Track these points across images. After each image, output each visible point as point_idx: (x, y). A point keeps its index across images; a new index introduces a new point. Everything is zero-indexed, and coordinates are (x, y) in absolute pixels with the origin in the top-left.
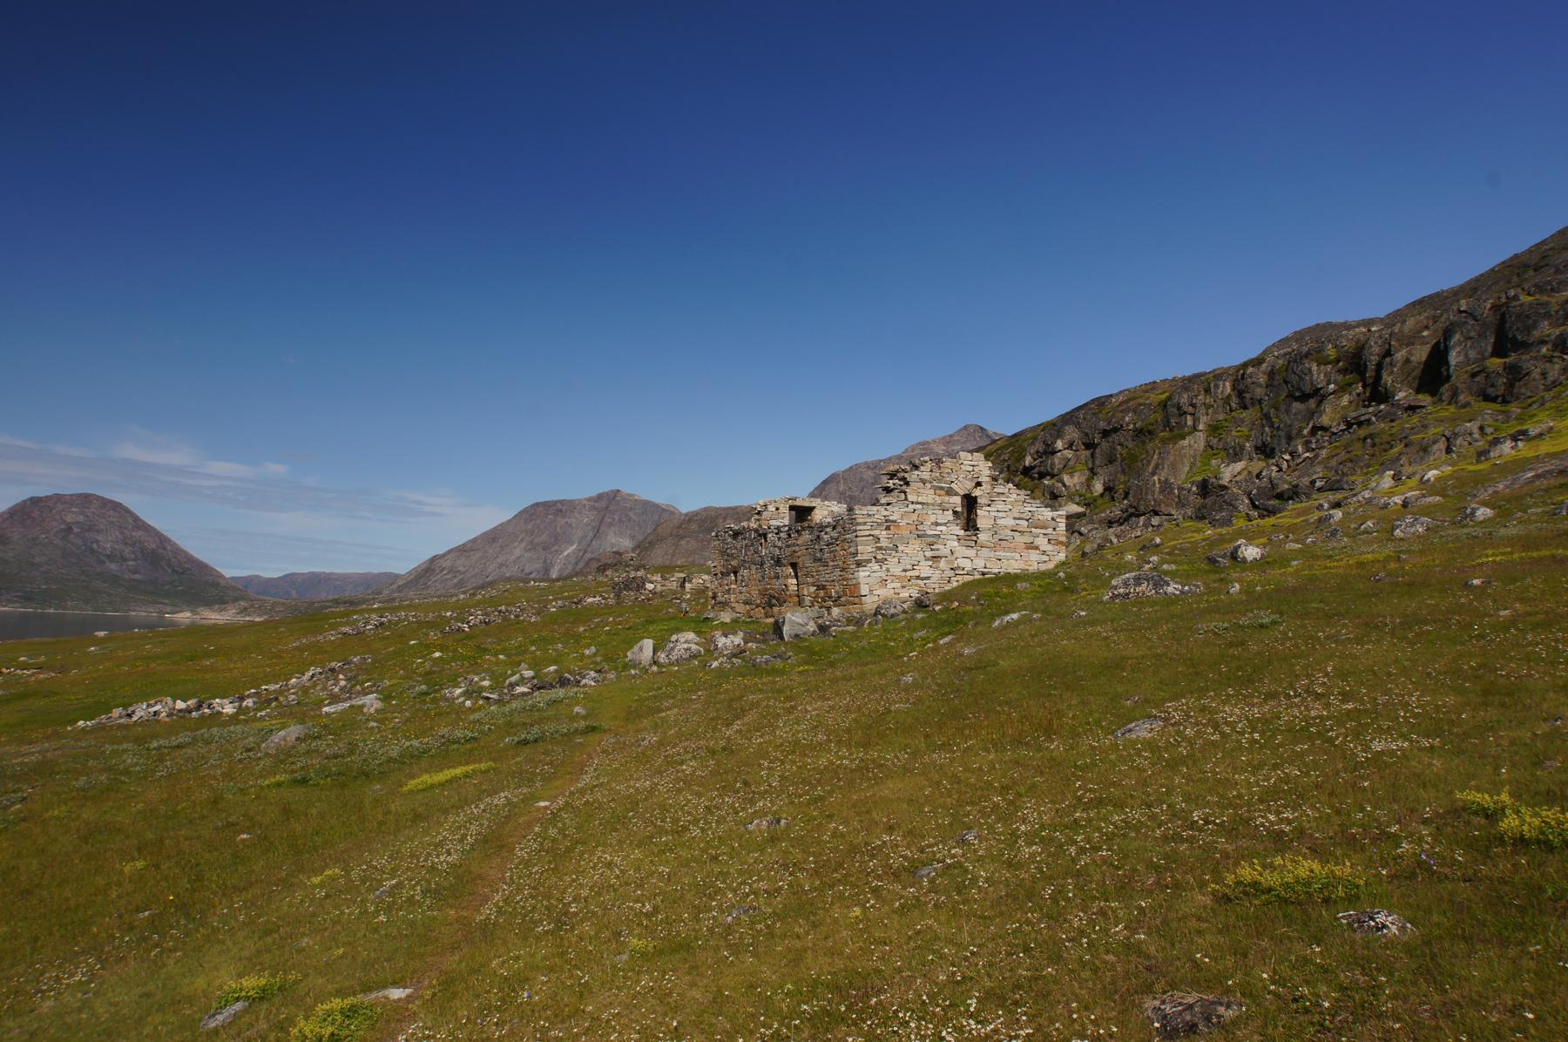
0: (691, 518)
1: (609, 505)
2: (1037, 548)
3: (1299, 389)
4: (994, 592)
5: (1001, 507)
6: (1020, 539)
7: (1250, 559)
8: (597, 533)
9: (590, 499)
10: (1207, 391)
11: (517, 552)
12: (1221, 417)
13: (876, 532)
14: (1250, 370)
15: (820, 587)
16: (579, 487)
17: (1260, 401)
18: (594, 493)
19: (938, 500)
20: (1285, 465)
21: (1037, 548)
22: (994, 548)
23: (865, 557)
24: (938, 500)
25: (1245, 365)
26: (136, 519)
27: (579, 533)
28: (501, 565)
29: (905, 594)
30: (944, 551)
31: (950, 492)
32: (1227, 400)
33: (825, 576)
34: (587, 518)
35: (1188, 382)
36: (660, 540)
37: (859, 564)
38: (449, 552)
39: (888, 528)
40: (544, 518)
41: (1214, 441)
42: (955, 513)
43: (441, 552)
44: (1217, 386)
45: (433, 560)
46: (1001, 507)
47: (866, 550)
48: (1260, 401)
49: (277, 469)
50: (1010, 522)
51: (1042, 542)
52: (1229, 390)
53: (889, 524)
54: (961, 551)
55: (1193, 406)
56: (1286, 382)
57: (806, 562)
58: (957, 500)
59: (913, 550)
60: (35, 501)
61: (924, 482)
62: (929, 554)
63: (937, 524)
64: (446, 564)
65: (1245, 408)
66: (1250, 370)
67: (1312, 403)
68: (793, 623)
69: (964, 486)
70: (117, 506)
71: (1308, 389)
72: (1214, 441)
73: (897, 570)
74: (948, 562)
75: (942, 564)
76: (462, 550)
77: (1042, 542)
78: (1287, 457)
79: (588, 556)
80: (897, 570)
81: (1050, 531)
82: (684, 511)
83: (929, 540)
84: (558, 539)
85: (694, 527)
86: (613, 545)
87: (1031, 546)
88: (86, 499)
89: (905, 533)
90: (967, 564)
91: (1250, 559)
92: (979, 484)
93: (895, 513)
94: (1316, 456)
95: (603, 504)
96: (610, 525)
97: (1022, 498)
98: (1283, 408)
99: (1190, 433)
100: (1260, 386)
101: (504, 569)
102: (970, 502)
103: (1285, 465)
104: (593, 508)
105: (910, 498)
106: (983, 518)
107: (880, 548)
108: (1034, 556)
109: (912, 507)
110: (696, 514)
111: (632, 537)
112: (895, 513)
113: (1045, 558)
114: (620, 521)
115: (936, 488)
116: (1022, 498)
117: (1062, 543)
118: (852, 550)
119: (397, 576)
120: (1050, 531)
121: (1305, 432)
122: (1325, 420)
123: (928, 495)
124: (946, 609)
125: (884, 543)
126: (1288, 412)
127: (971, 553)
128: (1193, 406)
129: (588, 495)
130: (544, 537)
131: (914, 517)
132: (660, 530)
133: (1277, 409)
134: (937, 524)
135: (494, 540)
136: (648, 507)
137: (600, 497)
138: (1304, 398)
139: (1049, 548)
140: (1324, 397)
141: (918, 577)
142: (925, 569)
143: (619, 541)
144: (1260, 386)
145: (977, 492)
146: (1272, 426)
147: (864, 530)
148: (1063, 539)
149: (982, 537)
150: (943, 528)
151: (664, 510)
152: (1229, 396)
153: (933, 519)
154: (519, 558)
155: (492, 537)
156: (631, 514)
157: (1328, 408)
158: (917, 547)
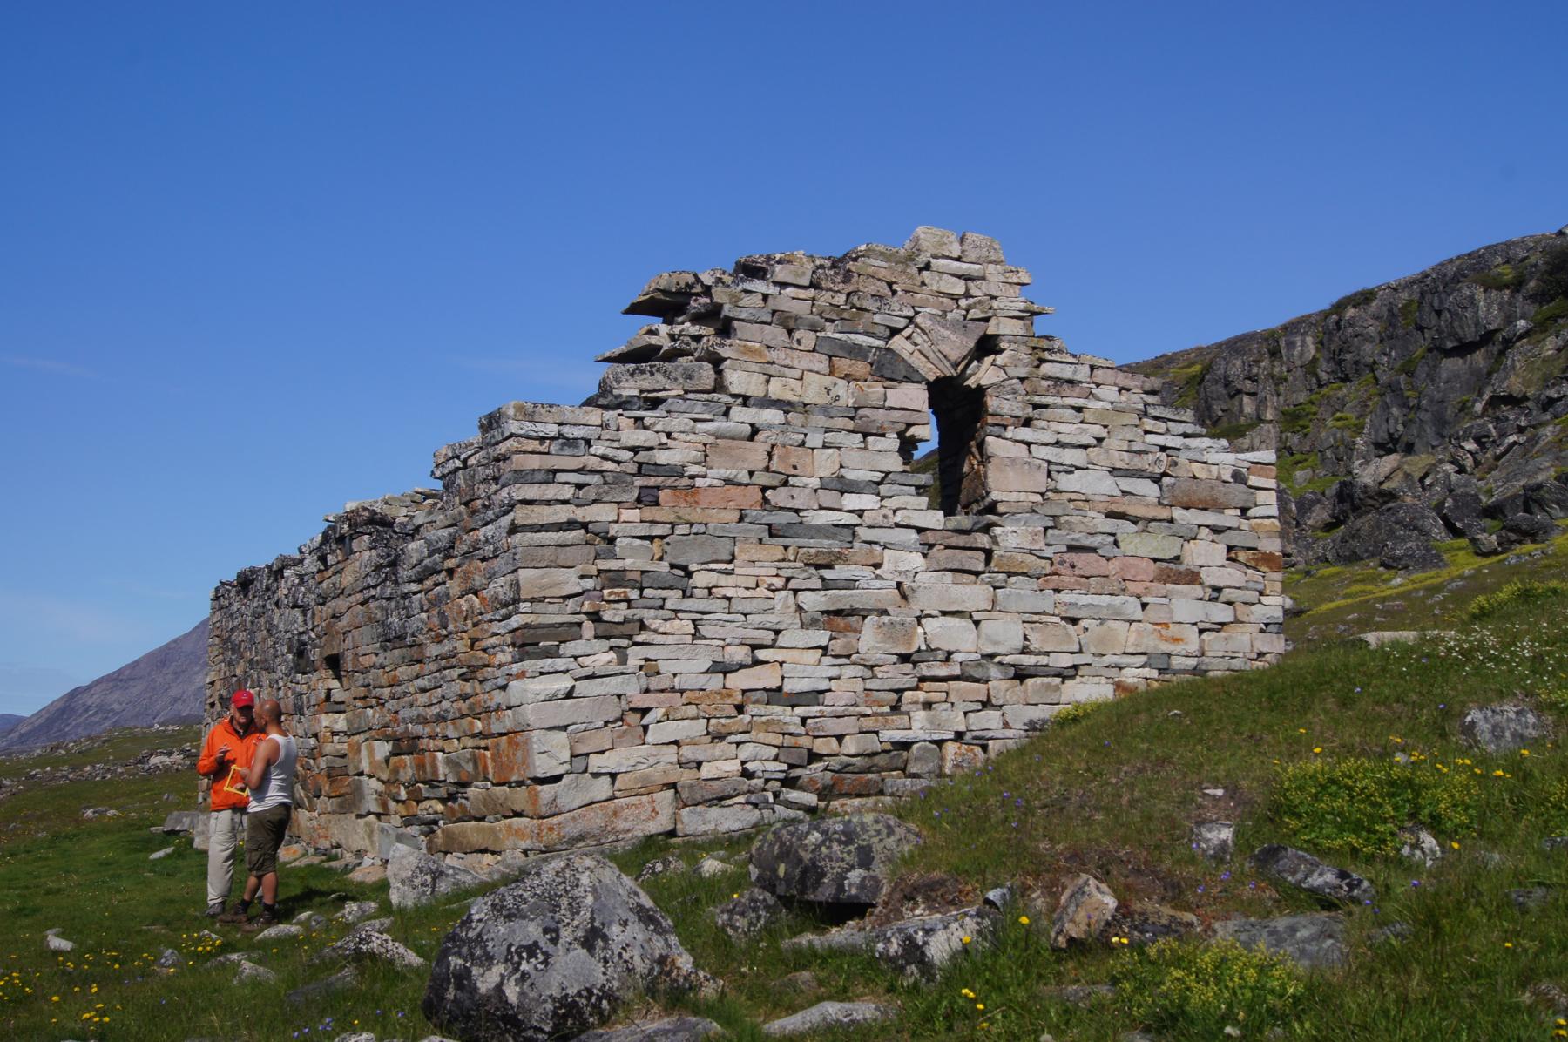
2: (1193, 577)
3: (1453, 335)
10: (1275, 353)
12: (1302, 397)
13: (601, 514)
14: (1350, 312)
15: (405, 745)
17: (1372, 367)
19: (846, 394)
20: (1469, 462)
21: (1193, 577)
22: (1049, 579)
23: (553, 615)
24: (846, 394)
25: (1340, 307)
28: (176, 700)
29: (722, 765)
30: (874, 589)
31: (889, 369)
32: (1311, 368)
33: (424, 695)
35: (1236, 346)
37: (528, 644)
38: (98, 682)
39: (648, 498)
41: (1294, 440)
42: (907, 445)
43: (85, 682)
44: (1291, 345)
46: (1070, 432)
48: (1372, 367)
50: (1100, 485)
51: (1206, 555)
52: (1311, 350)
53: (650, 482)
54: (936, 588)
55: (1253, 379)
56: (1421, 329)
57: (362, 647)
58: (915, 397)
59: (750, 584)
61: (789, 324)
62: (814, 601)
63: (844, 486)
64: (93, 700)
65: (1346, 379)
66: (1350, 312)
67: (1479, 358)
69: (935, 348)
71: (1470, 334)
72: (1294, 440)
74: (891, 632)
75: (869, 640)
76: (116, 680)
77: (1206, 555)
78: (1470, 446)
81: (1230, 517)
87: (1175, 572)
92: (987, 346)
94: (1534, 440)
97: (1136, 399)
98: (1422, 371)
99: (1251, 426)
100: (1370, 339)
101: (178, 706)
102: (960, 408)
103: (1469, 462)
105: (737, 380)
106: (1009, 467)
107: (616, 579)
108: (1186, 605)
113: (1221, 613)
115: (834, 352)
116: (1136, 399)
117: (1268, 559)
118: (500, 587)
119: (20, 720)
121: (1478, 407)
122: (1514, 384)
123: (810, 380)
124: (1010, 954)
125: (632, 558)
126: (1432, 377)
127: (974, 595)
128: (1253, 379)
131: (756, 454)
133: (1410, 374)
134: (844, 486)
138: (1464, 349)
139: (1231, 576)
140: (1508, 343)
141: (775, 695)
142: (802, 667)
144: (1370, 339)
145: (984, 374)
146: (1404, 404)
148: (1273, 546)
149: (1012, 537)
150: (867, 501)
152: (1314, 360)
153: (825, 463)
155: (162, 659)
157: (1516, 358)
158: (766, 571)
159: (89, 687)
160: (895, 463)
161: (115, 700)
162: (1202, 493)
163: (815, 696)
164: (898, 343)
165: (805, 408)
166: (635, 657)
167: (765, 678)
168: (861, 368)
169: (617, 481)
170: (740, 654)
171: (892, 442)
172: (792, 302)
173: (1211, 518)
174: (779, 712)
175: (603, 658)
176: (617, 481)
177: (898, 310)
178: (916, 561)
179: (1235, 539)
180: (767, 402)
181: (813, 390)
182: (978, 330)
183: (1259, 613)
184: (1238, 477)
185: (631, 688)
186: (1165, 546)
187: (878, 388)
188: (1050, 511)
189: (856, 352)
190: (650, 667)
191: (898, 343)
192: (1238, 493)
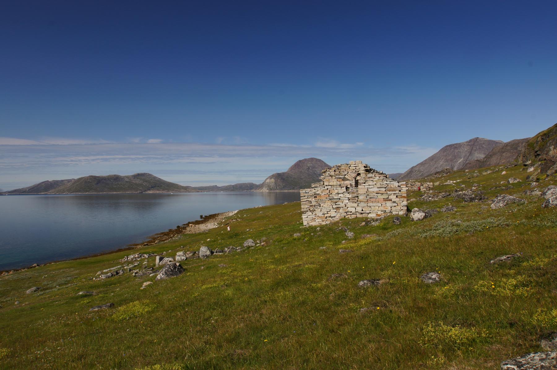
0: (507, 145)
1: (474, 143)
4: (361, 225)
5: (371, 183)
6: (381, 197)
7: (415, 219)
8: (471, 153)
9: (467, 142)
11: (441, 163)
13: (310, 199)
16: (461, 137)
18: (468, 139)
26: (325, 164)
27: (464, 154)
30: (342, 205)
34: (466, 149)
36: (495, 154)
38: (418, 165)
39: (315, 197)
40: (450, 151)
45: (412, 168)
46: (371, 183)
47: (304, 207)
49: (360, 144)
50: (376, 190)
51: (393, 197)
53: (315, 196)
59: (327, 206)
60: (300, 161)
61: (331, 176)
62: (334, 206)
63: (338, 194)
64: (417, 169)
68: (202, 251)
70: (320, 160)
73: (320, 214)
74: (344, 210)
75: (341, 210)
76: (422, 164)
77: (393, 197)
79: (468, 162)
80: (320, 214)
81: (397, 192)
82: (505, 142)
83: (334, 201)
84: (456, 157)
85: (509, 148)
86: (477, 157)
87: (388, 200)
88: (312, 159)
89: (324, 198)
90: (353, 210)
91: (415, 219)
93: (319, 191)
95: (472, 143)
96: (475, 150)
104: (468, 145)
105: (325, 184)
108: (389, 204)
109: (326, 187)
110: (510, 143)
111: (484, 154)
112: (319, 191)
114: (480, 148)
117: (404, 197)
119: (400, 174)
120: (397, 192)
123: (334, 182)
125: (314, 203)
129: (466, 141)
130: (450, 157)
132: (494, 151)
134: (338, 194)
135: (432, 160)
136: (490, 142)
137: (471, 141)
141: (330, 217)
142: (333, 213)
143: (480, 156)
145: (358, 178)
147: (303, 199)
150: (342, 195)
151: (497, 143)
153: (336, 191)
154: (442, 165)
155: (432, 159)
156: (484, 145)
158: (329, 204)
159: (416, 166)
160: (345, 190)
161: (422, 168)
162: (392, 189)
163: (335, 217)
164: (346, 176)
165: (334, 185)
166: (314, 213)
167: (329, 215)
168: (341, 180)
169: (312, 196)
170: (326, 212)
171: (345, 188)
172: (333, 173)
173: (394, 192)
174: (330, 218)
175: (310, 213)
176: (312, 196)
177: (346, 173)
178: (347, 201)
179: (398, 195)
180: (329, 185)
181: (335, 184)
182: (357, 173)
183: (402, 204)
184: (399, 186)
185: (314, 217)
186: (385, 196)
187: (343, 182)
188: (367, 193)
189: (340, 178)
190: (316, 214)
191: (346, 176)
192: (399, 188)
